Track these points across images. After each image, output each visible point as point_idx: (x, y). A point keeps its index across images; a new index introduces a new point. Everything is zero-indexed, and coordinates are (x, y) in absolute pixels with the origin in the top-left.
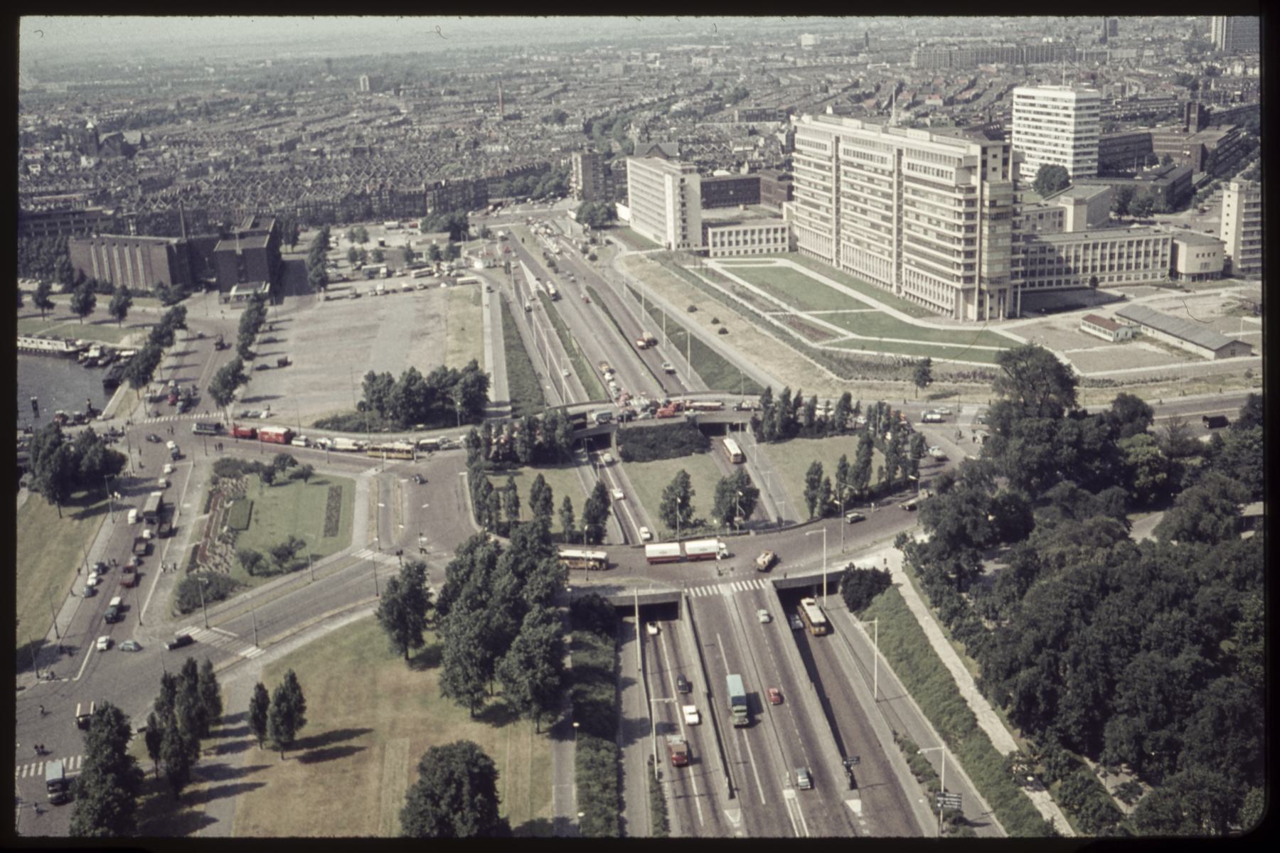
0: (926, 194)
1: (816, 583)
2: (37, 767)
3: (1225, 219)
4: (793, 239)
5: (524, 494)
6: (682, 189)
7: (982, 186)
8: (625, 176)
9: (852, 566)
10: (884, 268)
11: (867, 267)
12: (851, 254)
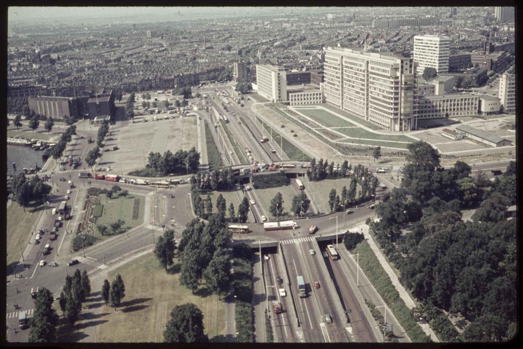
0: (378, 79)
1: (333, 238)
2: (15, 314)
3: (500, 90)
4: (324, 98)
5: (214, 202)
6: (279, 77)
7: (401, 76)
8: (256, 72)
9: (348, 231)
10: (361, 109)
11: (354, 109)
12: (348, 104)
